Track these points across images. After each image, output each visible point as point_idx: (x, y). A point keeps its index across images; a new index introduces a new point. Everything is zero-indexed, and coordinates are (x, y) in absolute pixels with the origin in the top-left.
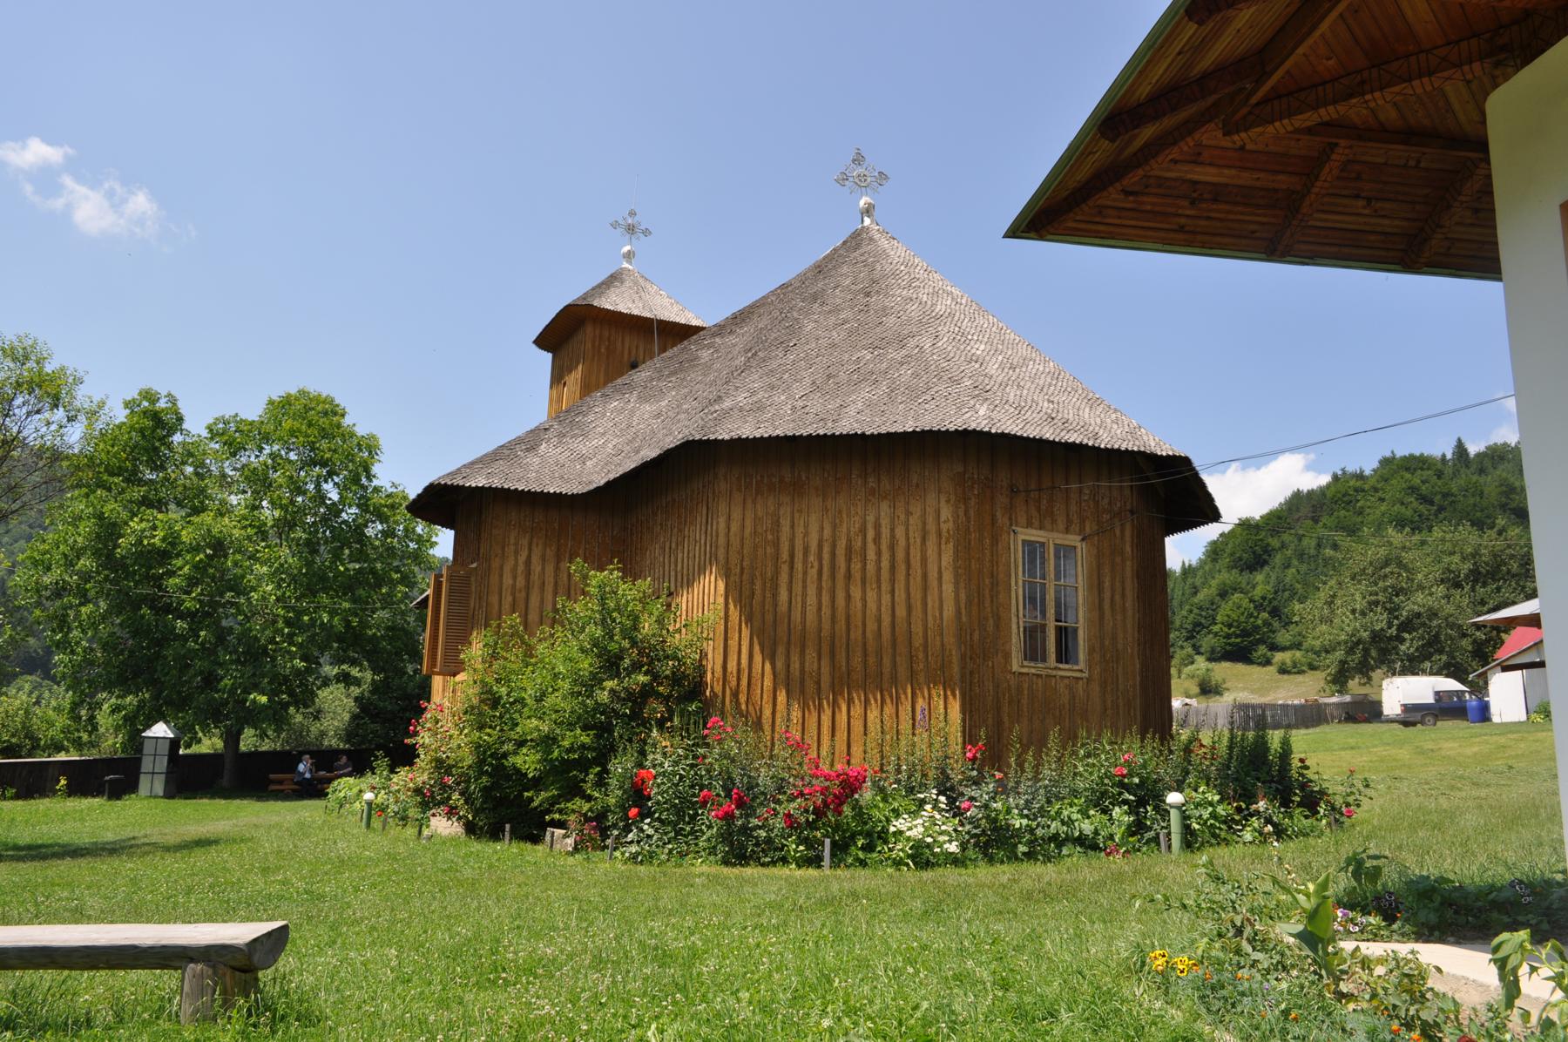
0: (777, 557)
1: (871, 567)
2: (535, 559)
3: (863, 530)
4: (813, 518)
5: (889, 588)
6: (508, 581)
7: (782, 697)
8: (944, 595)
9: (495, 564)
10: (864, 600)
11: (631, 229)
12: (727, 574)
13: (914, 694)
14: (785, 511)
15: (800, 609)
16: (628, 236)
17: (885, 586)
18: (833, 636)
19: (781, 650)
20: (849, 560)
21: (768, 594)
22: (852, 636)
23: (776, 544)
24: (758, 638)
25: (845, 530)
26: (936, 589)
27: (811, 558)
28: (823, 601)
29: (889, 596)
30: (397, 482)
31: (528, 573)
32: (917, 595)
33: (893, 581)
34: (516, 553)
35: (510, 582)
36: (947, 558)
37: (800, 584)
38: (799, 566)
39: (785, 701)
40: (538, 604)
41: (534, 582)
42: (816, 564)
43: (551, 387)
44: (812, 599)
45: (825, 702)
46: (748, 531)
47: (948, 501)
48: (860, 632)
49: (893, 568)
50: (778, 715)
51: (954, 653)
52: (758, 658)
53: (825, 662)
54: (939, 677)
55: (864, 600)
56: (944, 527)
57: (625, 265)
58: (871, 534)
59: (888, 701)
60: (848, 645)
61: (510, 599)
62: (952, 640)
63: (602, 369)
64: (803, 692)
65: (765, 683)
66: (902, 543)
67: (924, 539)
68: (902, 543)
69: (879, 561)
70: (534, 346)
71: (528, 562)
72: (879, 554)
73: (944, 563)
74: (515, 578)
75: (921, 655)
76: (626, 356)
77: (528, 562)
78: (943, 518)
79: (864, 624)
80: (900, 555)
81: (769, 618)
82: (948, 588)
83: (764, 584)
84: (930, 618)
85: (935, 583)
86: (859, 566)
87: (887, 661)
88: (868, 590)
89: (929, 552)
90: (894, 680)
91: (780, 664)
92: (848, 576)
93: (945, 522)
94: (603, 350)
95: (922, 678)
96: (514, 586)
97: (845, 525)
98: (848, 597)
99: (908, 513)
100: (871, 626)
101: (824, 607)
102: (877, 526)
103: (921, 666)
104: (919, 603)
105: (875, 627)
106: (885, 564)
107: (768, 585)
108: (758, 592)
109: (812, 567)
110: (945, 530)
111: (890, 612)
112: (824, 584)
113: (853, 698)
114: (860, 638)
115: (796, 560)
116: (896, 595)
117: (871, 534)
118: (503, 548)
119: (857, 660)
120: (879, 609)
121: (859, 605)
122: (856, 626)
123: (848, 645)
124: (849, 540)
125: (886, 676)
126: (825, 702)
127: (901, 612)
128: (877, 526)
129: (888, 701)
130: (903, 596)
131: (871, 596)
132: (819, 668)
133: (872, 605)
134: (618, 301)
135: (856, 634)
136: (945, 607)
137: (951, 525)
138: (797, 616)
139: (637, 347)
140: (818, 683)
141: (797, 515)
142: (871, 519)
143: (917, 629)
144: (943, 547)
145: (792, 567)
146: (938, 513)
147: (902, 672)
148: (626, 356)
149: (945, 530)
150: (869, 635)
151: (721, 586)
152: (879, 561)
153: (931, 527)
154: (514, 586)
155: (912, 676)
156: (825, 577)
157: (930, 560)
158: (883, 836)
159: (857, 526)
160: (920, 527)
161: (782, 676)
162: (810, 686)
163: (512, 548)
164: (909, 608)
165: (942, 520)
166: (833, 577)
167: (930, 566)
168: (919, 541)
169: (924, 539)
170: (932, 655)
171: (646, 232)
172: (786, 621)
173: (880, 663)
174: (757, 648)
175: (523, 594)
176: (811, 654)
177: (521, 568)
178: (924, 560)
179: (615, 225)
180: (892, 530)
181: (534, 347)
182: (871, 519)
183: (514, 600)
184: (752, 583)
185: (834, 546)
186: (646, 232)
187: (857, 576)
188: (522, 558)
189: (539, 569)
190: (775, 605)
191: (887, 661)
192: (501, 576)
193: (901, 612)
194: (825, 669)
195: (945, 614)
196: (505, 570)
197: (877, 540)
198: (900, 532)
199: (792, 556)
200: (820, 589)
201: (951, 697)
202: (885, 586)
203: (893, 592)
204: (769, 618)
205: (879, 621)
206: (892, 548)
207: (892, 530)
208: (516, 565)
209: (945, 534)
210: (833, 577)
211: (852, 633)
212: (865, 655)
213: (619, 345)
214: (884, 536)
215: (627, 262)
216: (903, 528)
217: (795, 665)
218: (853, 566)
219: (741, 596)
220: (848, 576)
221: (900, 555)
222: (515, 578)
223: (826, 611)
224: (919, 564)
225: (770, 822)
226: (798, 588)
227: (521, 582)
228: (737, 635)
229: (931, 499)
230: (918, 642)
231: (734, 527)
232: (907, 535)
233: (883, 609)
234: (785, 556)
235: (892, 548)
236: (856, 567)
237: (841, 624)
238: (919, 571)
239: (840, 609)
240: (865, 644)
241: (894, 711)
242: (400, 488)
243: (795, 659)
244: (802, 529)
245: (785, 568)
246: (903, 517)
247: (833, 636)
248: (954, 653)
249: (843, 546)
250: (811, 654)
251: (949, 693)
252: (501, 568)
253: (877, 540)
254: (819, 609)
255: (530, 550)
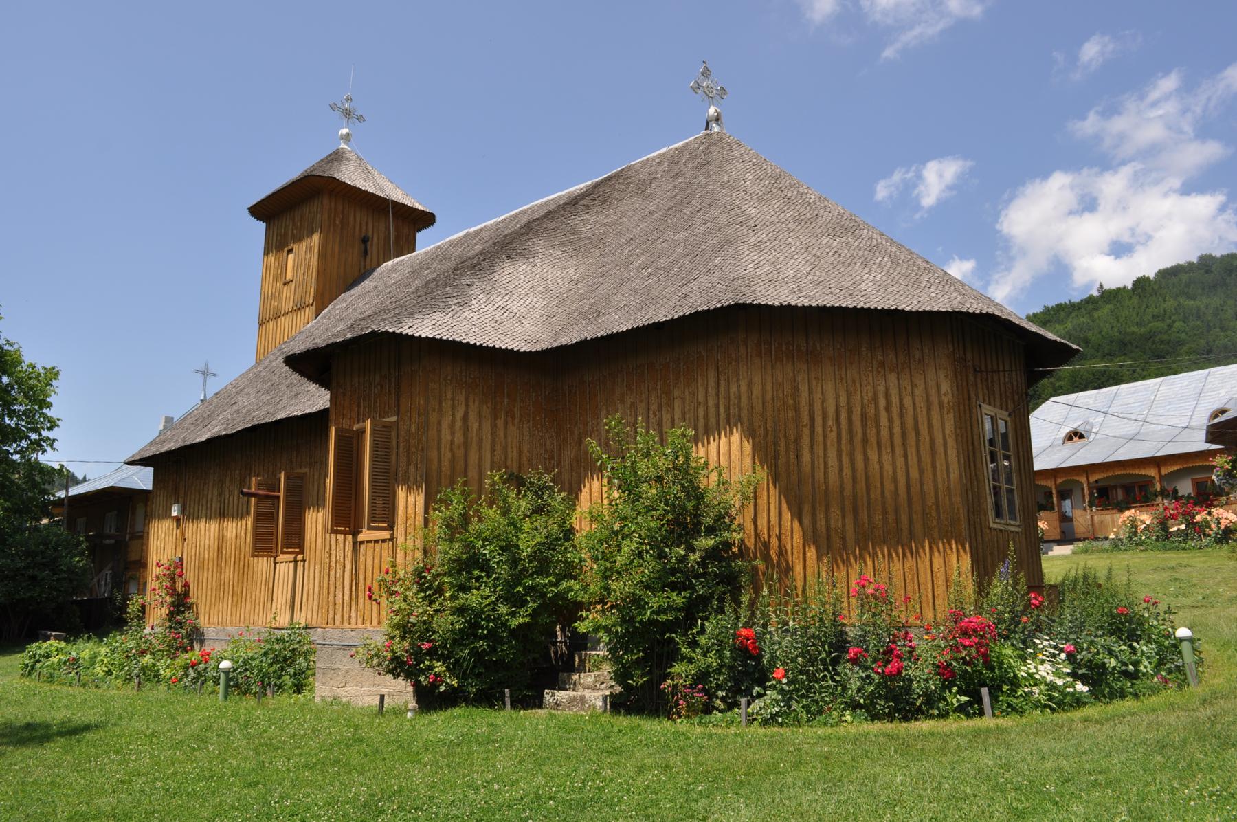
0: (797, 419)
1: (884, 433)
2: (473, 416)
3: (875, 399)
4: (829, 387)
5: (902, 452)
6: (446, 436)
7: (812, 553)
8: (949, 459)
9: (433, 418)
10: (880, 462)
11: (347, 113)
12: (750, 433)
13: (931, 548)
14: (802, 378)
15: (822, 470)
16: (345, 120)
17: (899, 450)
18: (855, 495)
19: (807, 508)
20: (864, 426)
21: (792, 456)
22: (872, 496)
23: (796, 408)
24: (785, 497)
25: (859, 398)
26: (943, 454)
27: (830, 423)
28: (844, 463)
29: (903, 459)
30: (12, 341)
31: (466, 429)
32: (927, 460)
33: (904, 445)
34: (453, 408)
35: (449, 438)
36: (949, 427)
37: (821, 447)
38: (819, 429)
39: (815, 556)
40: (477, 461)
41: (472, 438)
42: (835, 428)
43: (267, 252)
44: (833, 460)
45: (851, 557)
46: (769, 395)
47: (946, 376)
48: (879, 491)
49: (904, 434)
50: (809, 570)
51: (961, 511)
52: (787, 516)
53: (849, 520)
54: (946, 534)
55: (880, 462)
56: (945, 399)
57: (343, 146)
58: (882, 403)
59: (908, 555)
60: (869, 503)
61: (449, 455)
62: (959, 499)
63: (338, 240)
64: (829, 547)
65: (795, 539)
66: (910, 411)
67: (929, 409)
68: (910, 411)
69: (891, 428)
70: (247, 212)
71: (465, 418)
72: (890, 420)
73: (947, 432)
74: (453, 434)
75: (934, 514)
76: (357, 233)
77: (465, 418)
78: (943, 391)
79: (882, 484)
80: (910, 422)
81: (795, 478)
82: (952, 453)
83: (787, 446)
84: (939, 480)
85: (941, 450)
86: (874, 431)
87: (904, 518)
88: (884, 453)
89: (934, 421)
90: (912, 536)
91: (806, 521)
92: (865, 440)
93: (945, 395)
94: (337, 222)
95: (936, 535)
96: (452, 442)
97: (859, 393)
98: (866, 459)
99: (913, 386)
100: (889, 487)
101: (844, 469)
102: (887, 395)
103: (935, 522)
104: (929, 465)
105: (892, 488)
106: (897, 430)
107: (792, 447)
108: (782, 453)
109: (831, 431)
110: (946, 402)
111: (904, 474)
112: (843, 447)
113: (876, 553)
114: (879, 497)
115: (816, 423)
116: (909, 458)
117: (882, 403)
118: (440, 403)
119: (878, 517)
120: (894, 472)
121: (877, 467)
122: (875, 487)
123: (869, 503)
124: (863, 407)
125: (905, 532)
126: (851, 557)
127: (914, 474)
128: (887, 395)
129: (908, 555)
130: (915, 460)
131: (887, 458)
132: (844, 526)
133: (888, 468)
134: (350, 175)
135: (875, 494)
136: (951, 470)
137: (950, 396)
138: (819, 475)
139: (367, 223)
140: (843, 539)
141: (814, 382)
142: (881, 389)
143: (928, 488)
144: (946, 416)
145: (918, 434)
146: (938, 385)
147: (918, 528)
148: (357, 233)
149: (946, 402)
150: (888, 494)
151: (748, 447)
152: (891, 428)
153: (934, 399)
154: (452, 442)
155: (928, 532)
156: (844, 441)
157: (935, 428)
158: (1015, 683)
159: (870, 394)
160: (925, 398)
161: (810, 533)
162: (837, 543)
163: (450, 403)
164: (921, 472)
165: (943, 392)
166: (851, 440)
167: (936, 433)
168: (924, 410)
169: (929, 409)
170: (944, 513)
171: (361, 119)
172: (810, 481)
173: (898, 521)
174: (785, 506)
175: (462, 451)
176: (835, 512)
177: (459, 424)
178: (930, 427)
179: (333, 107)
180: (901, 400)
181: (247, 212)
182: (881, 389)
183: (453, 456)
184: (776, 444)
185: (850, 413)
186: (361, 119)
187: (874, 441)
188: (459, 414)
189: (476, 426)
190: (799, 465)
191: (904, 518)
192: (439, 431)
193: (914, 474)
194: (850, 527)
195: (952, 476)
196: (443, 426)
197: (888, 408)
198: (908, 402)
199: (812, 419)
200: (839, 451)
201: (961, 551)
202: (899, 450)
203: (906, 456)
204: (795, 478)
205: (895, 481)
206: (902, 416)
207: (901, 400)
208: (454, 420)
209: (946, 405)
210: (851, 440)
211: (872, 493)
212: (885, 512)
213: (351, 219)
214: (894, 405)
215: (345, 143)
216: (910, 398)
217: (822, 523)
218: (868, 431)
219: (766, 455)
220: (865, 440)
221: (910, 422)
222: (453, 434)
223: (847, 472)
224: (927, 432)
225: (921, 675)
226: (819, 450)
227: (459, 438)
228: (766, 494)
229: (931, 374)
230: (931, 501)
231: (756, 391)
232: (914, 404)
233: (898, 471)
234: (806, 420)
235: (902, 416)
236: (872, 432)
237: (862, 485)
238: (928, 438)
239: (860, 470)
240: (884, 504)
241: (942, 561)
242: (16, 347)
243: (821, 517)
244: (819, 395)
245: (806, 431)
246: (909, 388)
247: (855, 495)
248: (961, 511)
249: (859, 412)
250: (835, 512)
251: (960, 547)
252: (439, 423)
253: (888, 408)
254: (841, 470)
255: (467, 405)
